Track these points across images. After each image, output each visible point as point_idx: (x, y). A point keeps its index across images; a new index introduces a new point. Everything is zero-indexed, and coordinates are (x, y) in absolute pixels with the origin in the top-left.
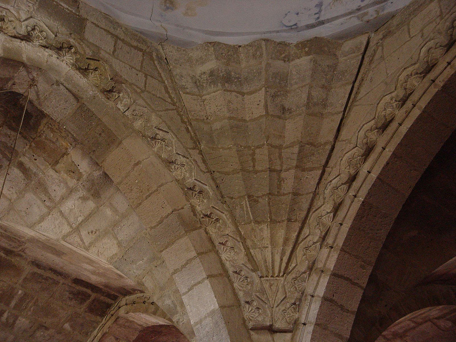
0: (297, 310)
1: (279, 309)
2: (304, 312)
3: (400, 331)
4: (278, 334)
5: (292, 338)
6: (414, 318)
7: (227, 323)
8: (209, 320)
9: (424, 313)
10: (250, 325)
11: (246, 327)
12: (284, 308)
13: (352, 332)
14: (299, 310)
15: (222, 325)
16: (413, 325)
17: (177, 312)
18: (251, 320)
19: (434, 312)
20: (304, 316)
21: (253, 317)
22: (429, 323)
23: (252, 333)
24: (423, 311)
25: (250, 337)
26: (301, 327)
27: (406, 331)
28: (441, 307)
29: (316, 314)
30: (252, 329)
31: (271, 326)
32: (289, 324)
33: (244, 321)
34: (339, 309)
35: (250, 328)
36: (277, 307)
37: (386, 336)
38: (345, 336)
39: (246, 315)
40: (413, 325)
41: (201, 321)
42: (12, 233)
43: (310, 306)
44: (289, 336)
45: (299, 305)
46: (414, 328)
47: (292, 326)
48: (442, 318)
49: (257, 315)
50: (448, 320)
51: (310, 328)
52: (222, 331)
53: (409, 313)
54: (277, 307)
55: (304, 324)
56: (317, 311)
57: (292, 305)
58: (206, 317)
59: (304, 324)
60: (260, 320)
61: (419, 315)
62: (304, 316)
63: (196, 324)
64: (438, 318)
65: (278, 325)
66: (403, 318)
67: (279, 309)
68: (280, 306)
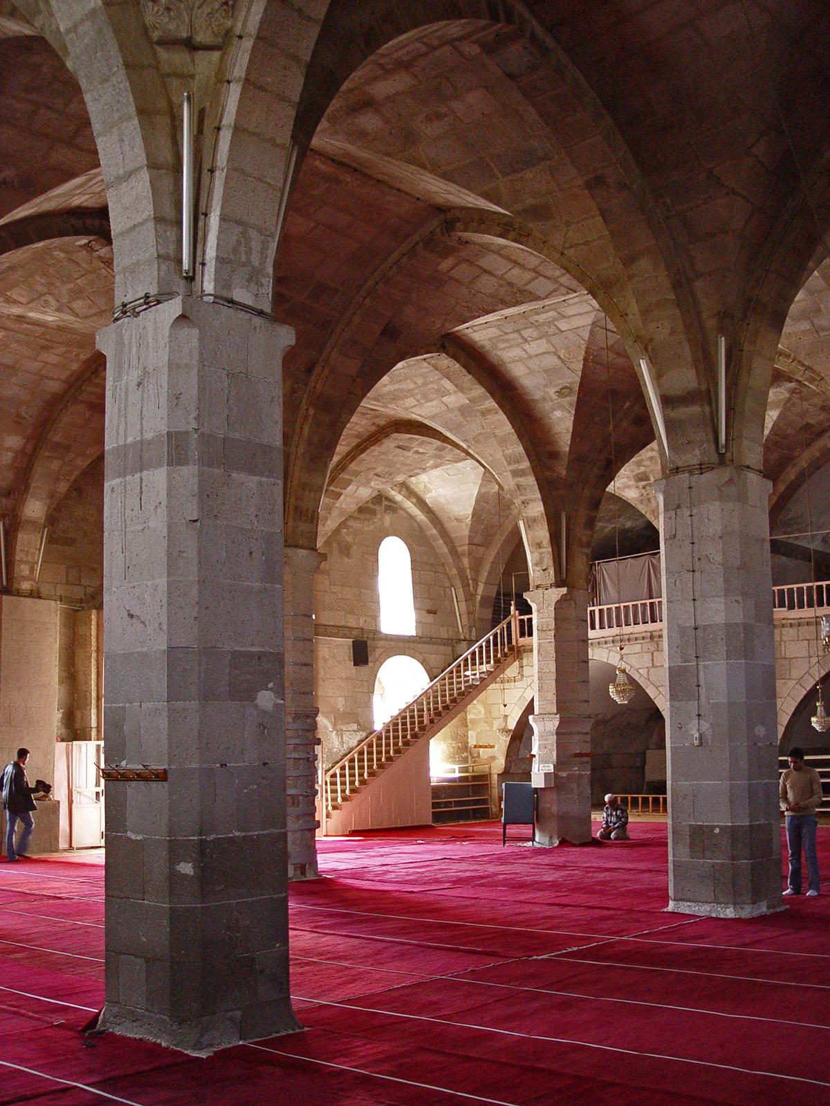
0: (230, 15)
1: (203, 13)
2: (241, 18)
3: (405, 59)
4: (201, 52)
5: (222, 59)
6: (425, 36)
7: (117, 31)
8: (87, 24)
9: (438, 30)
10: (156, 35)
11: (149, 39)
12: (209, 10)
13: (315, 52)
14: (232, 14)
15: (109, 33)
16: (424, 49)
17: (40, 12)
18: (157, 28)
19: (454, 28)
20: (240, 25)
21: (159, 23)
22: (448, 48)
23: (158, 49)
24: (435, 26)
25: (155, 53)
26: (235, 41)
27: (414, 59)
28: (463, 21)
29: (259, 21)
30: (159, 43)
31: (190, 39)
32: (216, 36)
33: (145, 29)
34: (296, 14)
35: (155, 39)
36: (199, 8)
37: (386, 66)
38: (303, 57)
39: (149, 19)
40: (424, 49)
41: (75, 28)
42: (718, 420)
43: (249, 9)
44: (216, 55)
45: (233, 7)
46: (424, 55)
47: (220, 40)
48: (466, 39)
49: (166, 20)
50: (474, 42)
51: (248, 44)
52: (109, 45)
53: (413, 28)
54: (199, 8)
55: (240, 37)
56: (260, 16)
57: (222, 6)
58: (83, 20)
59: (240, 37)
60: (171, 28)
61: (431, 33)
62: (240, 25)
63: (68, 31)
64: (459, 39)
65: (200, 38)
66: (404, 36)
67: (203, 13)
68: (204, 7)
